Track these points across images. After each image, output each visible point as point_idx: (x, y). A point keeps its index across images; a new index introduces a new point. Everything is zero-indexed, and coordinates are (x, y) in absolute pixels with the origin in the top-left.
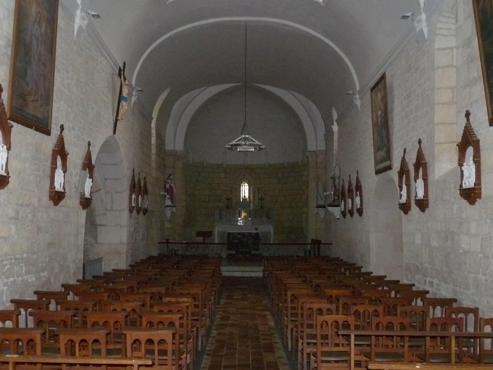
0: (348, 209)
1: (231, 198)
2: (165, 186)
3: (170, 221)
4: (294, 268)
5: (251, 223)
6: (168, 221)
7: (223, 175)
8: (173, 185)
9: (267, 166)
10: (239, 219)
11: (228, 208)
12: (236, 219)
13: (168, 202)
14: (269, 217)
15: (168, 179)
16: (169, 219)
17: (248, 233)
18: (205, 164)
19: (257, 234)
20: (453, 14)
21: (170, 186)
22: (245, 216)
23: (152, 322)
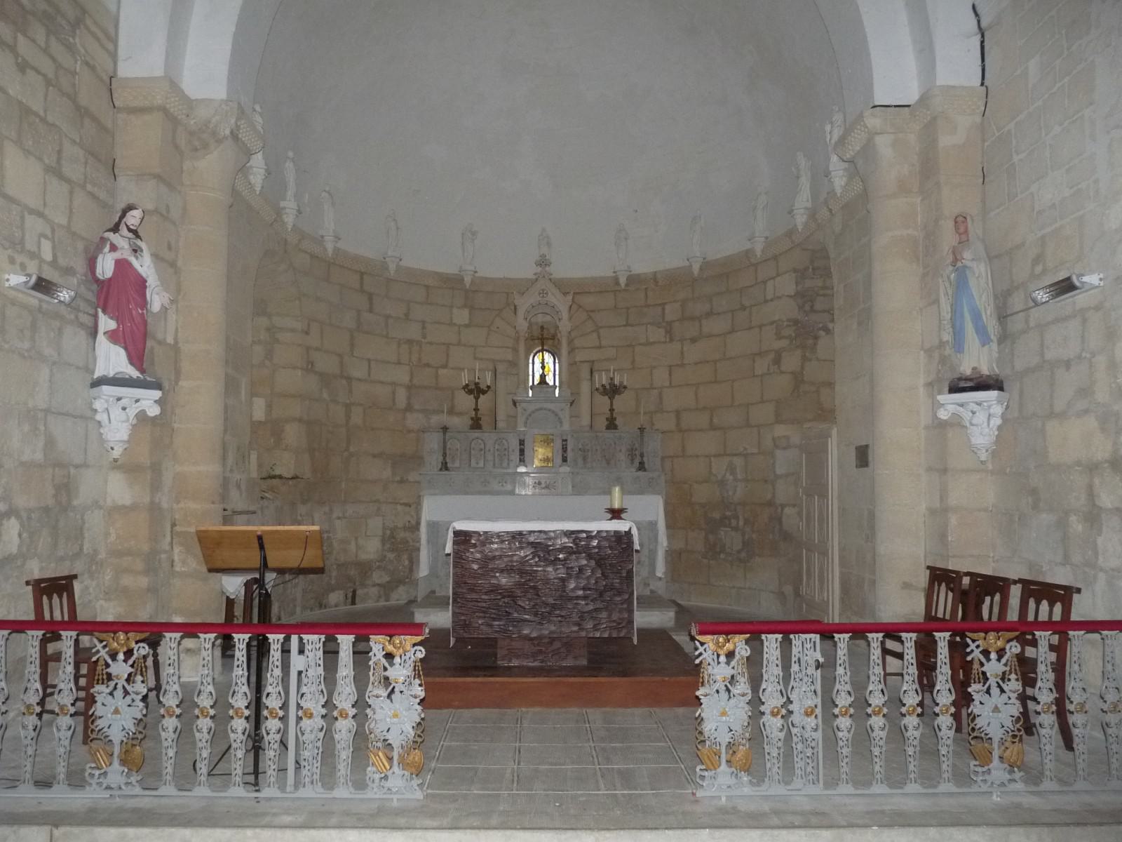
0: (104, 585)
1: (489, 387)
2: (92, 264)
3: (127, 467)
4: (618, 581)
5: (570, 487)
6: (116, 465)
7: (461, 316)
8: (144, 266)
9: (623, 281)
10: (522, 469)
11: (476, 424)
12: (510, 471)
13: (113, 359)
14: (642, 463)
15: (115, 229)
16: (117, 453)
17: (568, 534)
18: (392, 267)
19: (622, 540)
20: (655, 367)
21: (122, 265)
22: (547, 460)
23: (287, 749)
